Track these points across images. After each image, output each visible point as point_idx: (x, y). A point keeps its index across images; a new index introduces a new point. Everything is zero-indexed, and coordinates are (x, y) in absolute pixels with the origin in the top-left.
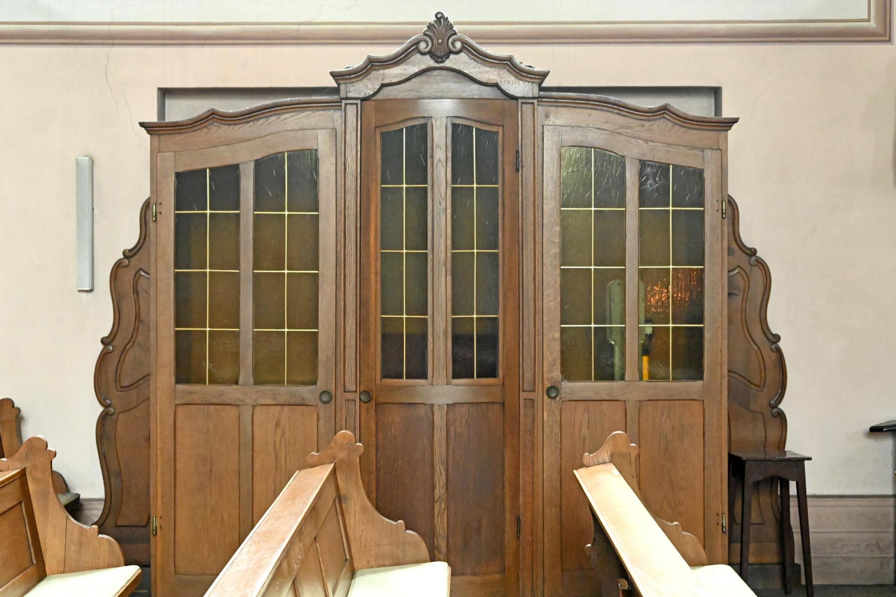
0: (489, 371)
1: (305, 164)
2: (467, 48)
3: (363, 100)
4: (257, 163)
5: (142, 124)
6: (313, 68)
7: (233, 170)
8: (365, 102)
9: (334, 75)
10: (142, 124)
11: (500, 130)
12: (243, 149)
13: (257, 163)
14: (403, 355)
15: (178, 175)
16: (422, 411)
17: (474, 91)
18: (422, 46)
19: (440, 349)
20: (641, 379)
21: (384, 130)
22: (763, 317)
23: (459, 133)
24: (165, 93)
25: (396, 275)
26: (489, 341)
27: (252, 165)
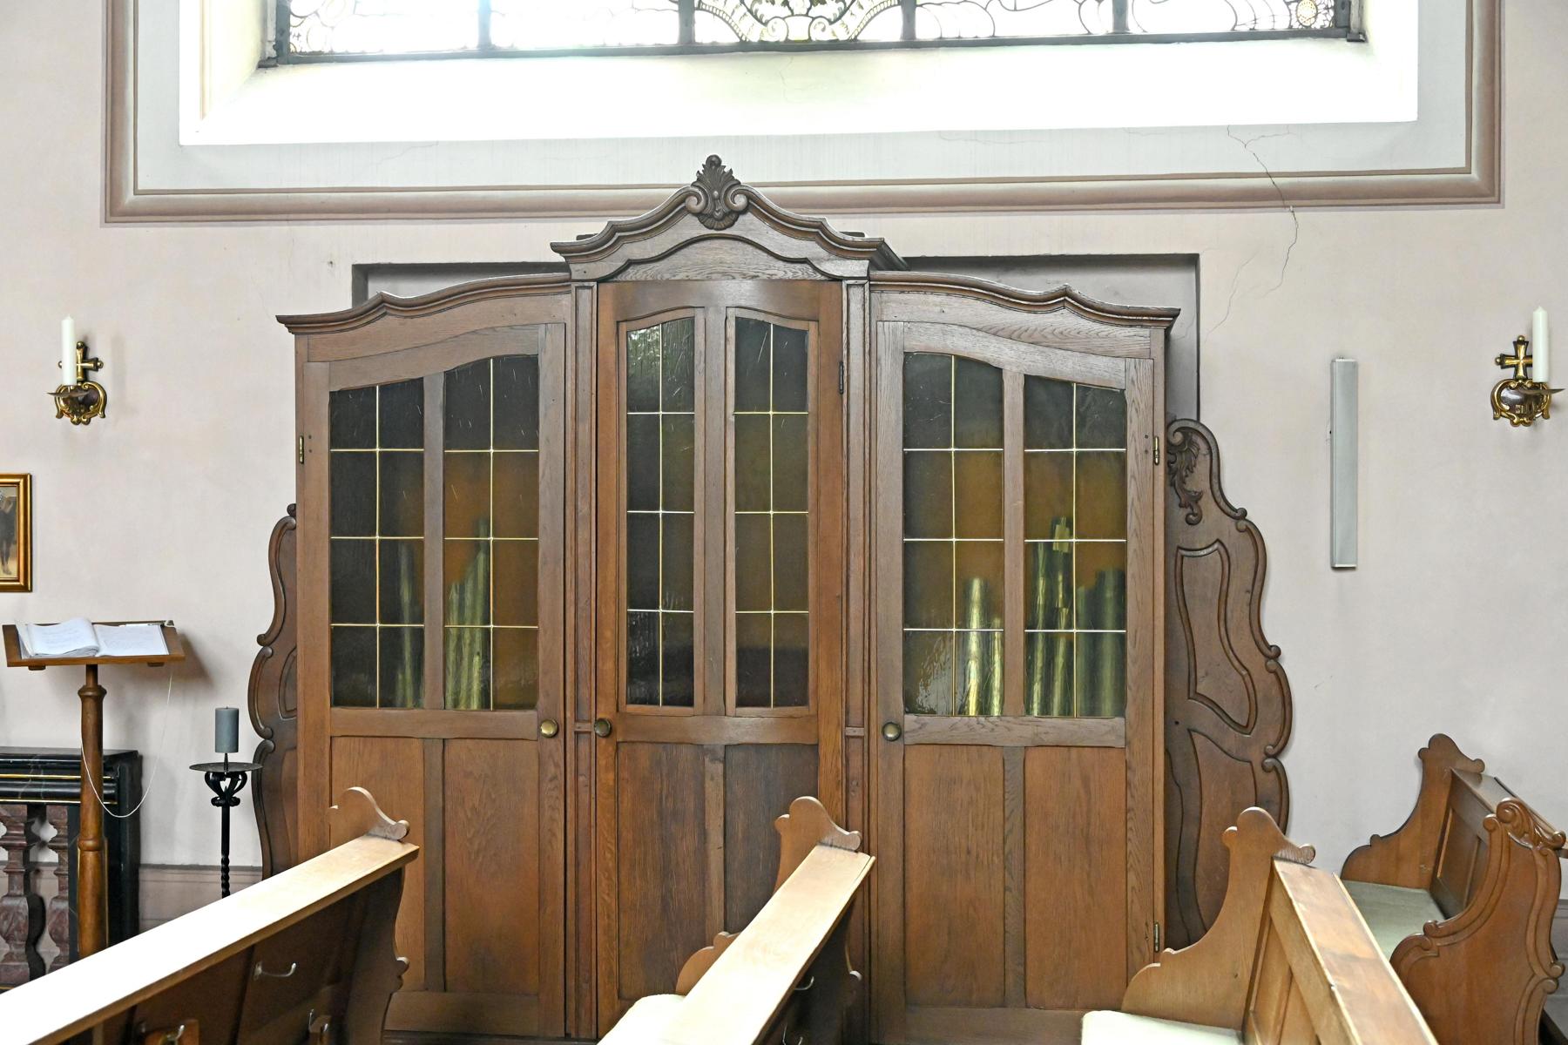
0: (794, 692)
1: (521, 372)
2: (754, 204)
3: (600, 281)
4: (449, 375)
5: (280, 319)
6: (531, 242)
7: (415, 387)
8: (602, 286)
9: (556, 248)
10: (280, 319)
11: (812, 326)
12: (424, 355)
13: (449, 375)
14: (661, 668)
15: (332, 393)
16: (686, 753)
17: (782, 271)
18: (693, 203)
19: (716, 664)
20: (1028, 711)
21: (623, 698)
22: (1258, 638)
23: (748, 330)
24: (363, 273)
25: (653, 557)
26: (795, 662)
27: (441, 381)
